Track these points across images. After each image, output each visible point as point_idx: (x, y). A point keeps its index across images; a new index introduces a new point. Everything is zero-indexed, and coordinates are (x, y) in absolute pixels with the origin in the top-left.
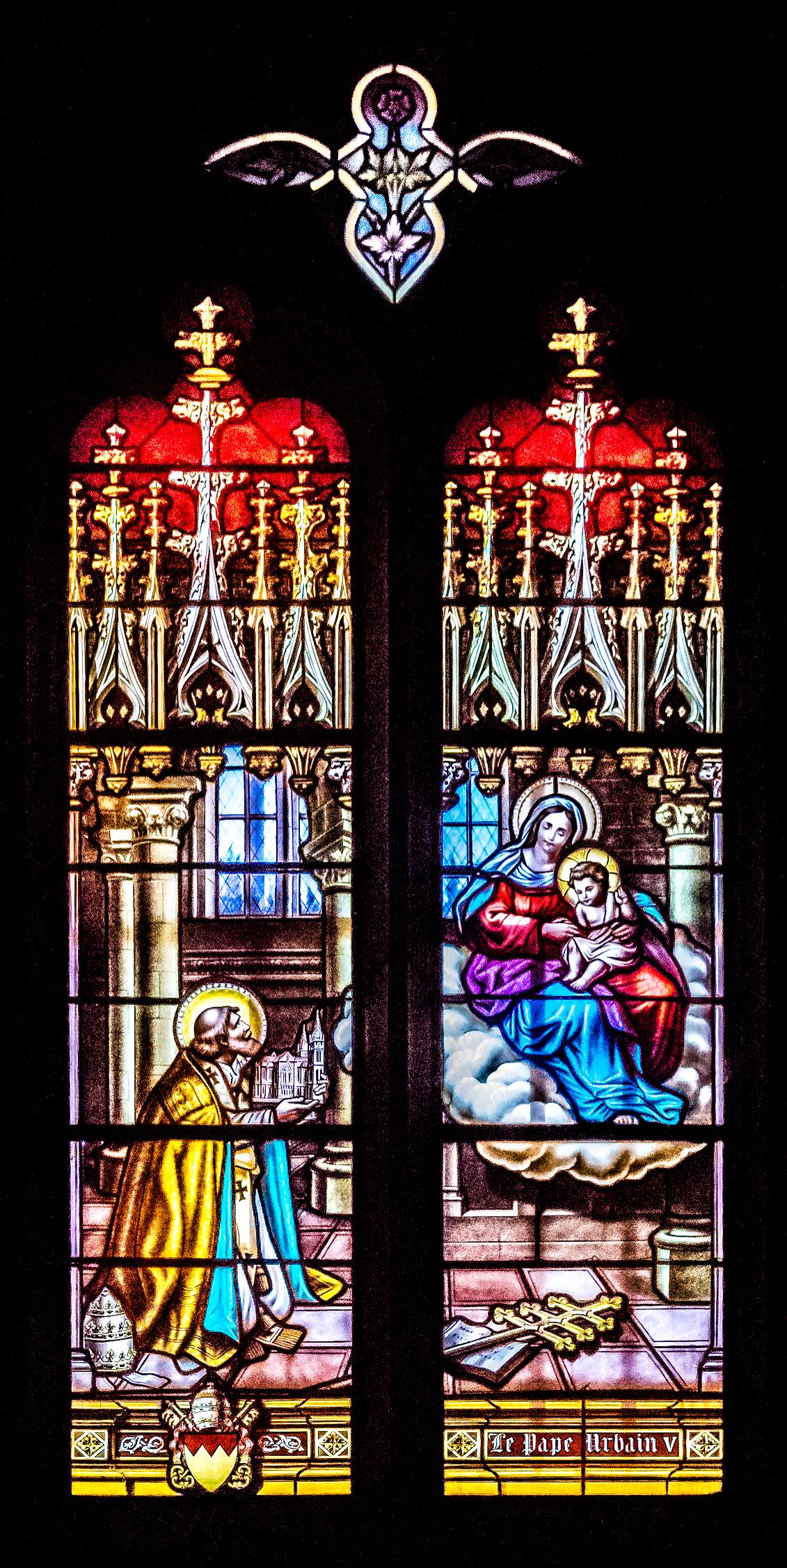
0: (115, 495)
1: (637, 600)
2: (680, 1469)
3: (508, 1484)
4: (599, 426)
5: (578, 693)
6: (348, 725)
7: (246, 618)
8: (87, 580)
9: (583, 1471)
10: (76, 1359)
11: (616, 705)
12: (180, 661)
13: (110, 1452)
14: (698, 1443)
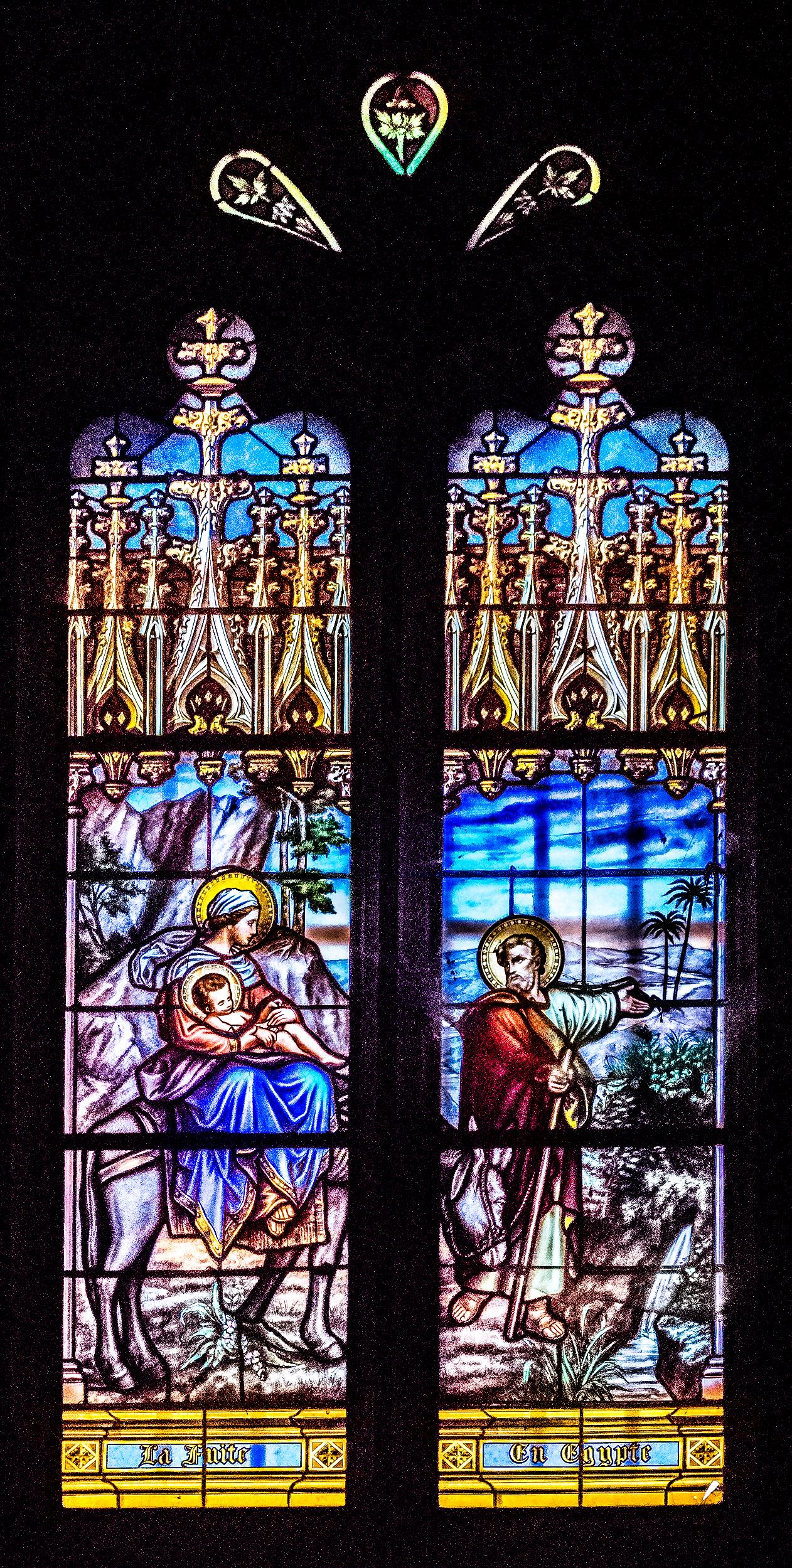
1: (344, 608)
3: (504, 1496)
4: (606, 430)
5: (579, 695)
6: (722, 728)
7: (246, 626)
9: (580, 1483)
13: (101, 1464)
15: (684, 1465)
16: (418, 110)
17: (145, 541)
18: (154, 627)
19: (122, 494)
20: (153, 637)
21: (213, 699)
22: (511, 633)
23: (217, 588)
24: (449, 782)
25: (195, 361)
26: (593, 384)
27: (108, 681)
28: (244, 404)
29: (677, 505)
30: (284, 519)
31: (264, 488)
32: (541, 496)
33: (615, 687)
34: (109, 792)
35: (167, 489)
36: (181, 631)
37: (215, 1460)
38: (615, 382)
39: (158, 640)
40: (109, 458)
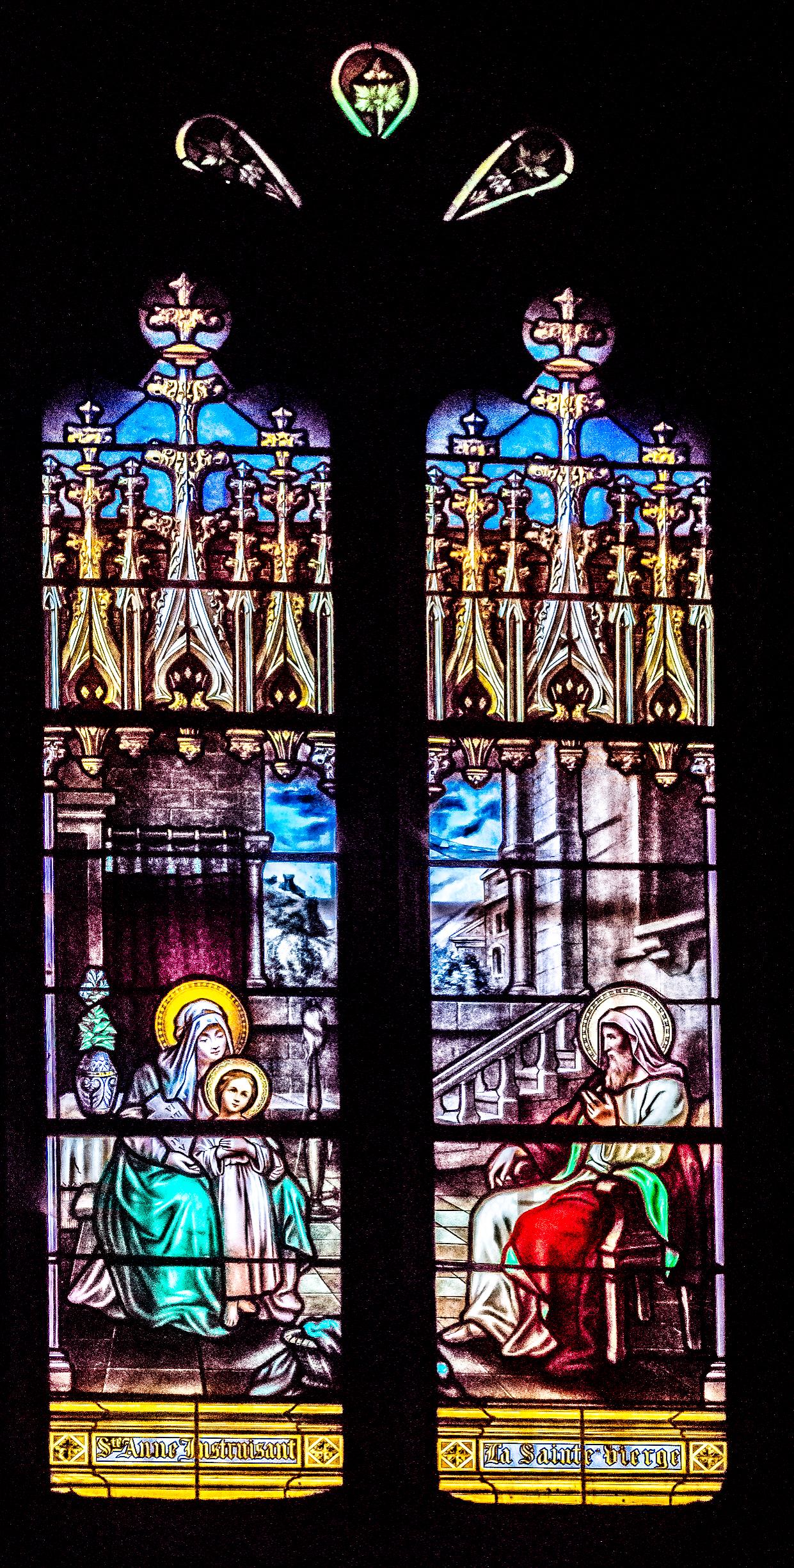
0: (89, 473)
2: (680, 1483)
4: (585, 417)
5: (564, 688)
6: (711, 722)
8: (59, 558)
10: (55, 1358)
11: (223, 688)
12: (156, 643)
14: (61, 1447)
15: (688, 1469)
16: (395, 80)
17: (122, 511)
18: (514, 609)
19: (479, 474)
20: (703, 627)
21: (574, 689)
22: (111, 609)
23: (578, 574)
24: (50, 758)
25: (170, 327)
26: (189, 355)
27: (467, 664)
28: (220, 374)
29: (278, 482)
30: (453, 500)
31: (435, 467)
32: (138, 469)
33: (599, 682)
34: (470, 778)
35: (526, 471)
36: (541, 616)
37: (568, 1461)
38: (212, 354)
39: (53, 613)
40: (275, 430)
